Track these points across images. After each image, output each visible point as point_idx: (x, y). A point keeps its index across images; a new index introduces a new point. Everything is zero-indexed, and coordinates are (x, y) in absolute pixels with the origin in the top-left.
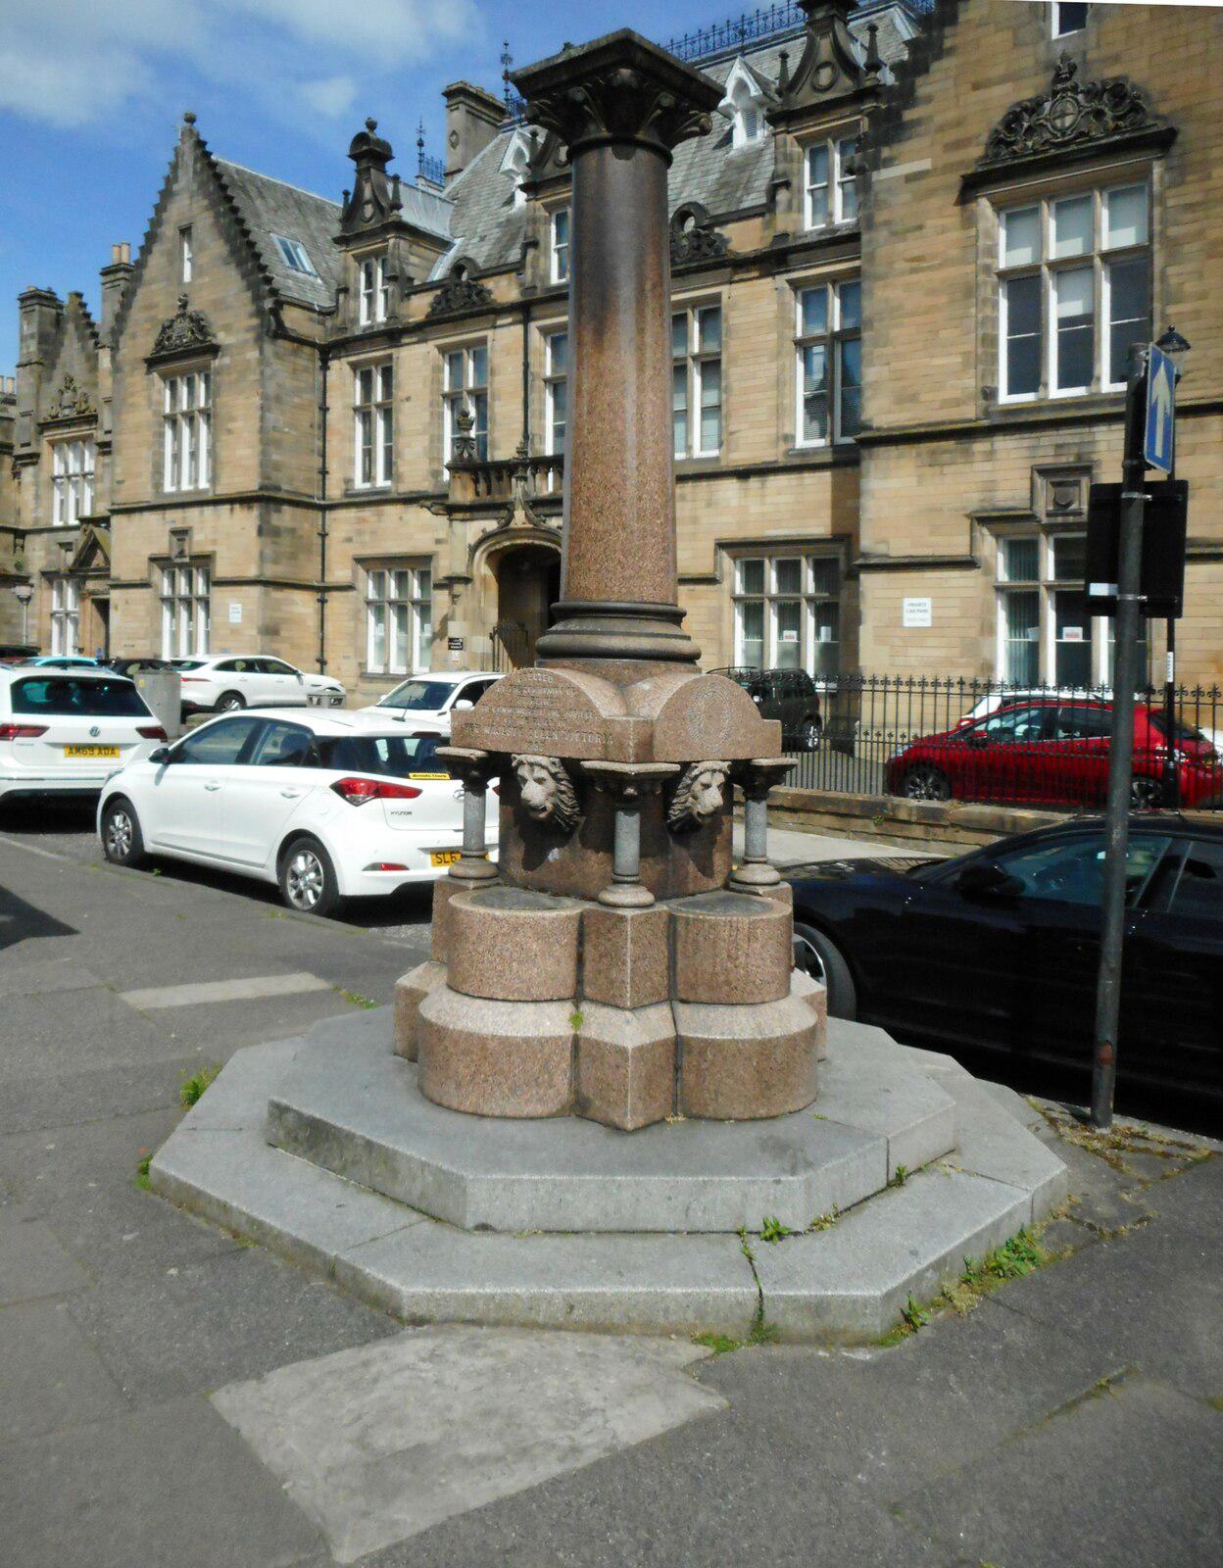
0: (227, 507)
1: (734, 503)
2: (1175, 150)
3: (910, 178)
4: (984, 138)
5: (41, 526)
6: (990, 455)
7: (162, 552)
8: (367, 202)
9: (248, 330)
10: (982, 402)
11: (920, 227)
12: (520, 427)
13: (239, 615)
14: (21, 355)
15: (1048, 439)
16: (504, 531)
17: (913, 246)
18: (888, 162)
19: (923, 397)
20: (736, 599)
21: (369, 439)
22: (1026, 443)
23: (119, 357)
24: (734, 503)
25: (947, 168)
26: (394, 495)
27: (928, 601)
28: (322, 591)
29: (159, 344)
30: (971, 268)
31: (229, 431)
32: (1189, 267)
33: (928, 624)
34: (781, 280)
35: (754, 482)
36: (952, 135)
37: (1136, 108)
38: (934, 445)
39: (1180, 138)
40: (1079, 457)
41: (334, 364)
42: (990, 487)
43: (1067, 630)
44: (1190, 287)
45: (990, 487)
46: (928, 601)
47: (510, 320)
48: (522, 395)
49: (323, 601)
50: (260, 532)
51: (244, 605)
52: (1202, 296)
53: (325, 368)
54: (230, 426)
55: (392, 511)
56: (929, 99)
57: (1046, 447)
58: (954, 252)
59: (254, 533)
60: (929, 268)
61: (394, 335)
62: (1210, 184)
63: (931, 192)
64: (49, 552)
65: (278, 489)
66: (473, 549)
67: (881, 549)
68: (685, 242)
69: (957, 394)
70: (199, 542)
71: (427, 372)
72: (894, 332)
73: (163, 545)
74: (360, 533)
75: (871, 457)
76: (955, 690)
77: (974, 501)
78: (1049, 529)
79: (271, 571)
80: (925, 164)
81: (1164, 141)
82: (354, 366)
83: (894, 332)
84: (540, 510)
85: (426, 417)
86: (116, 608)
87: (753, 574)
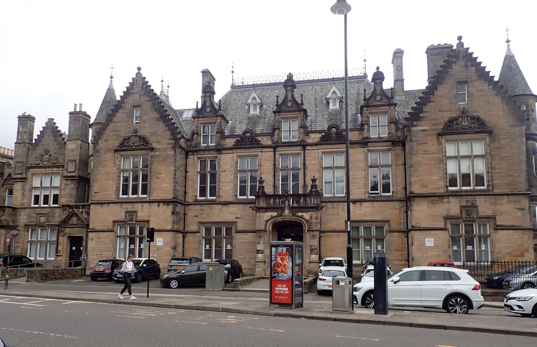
0: (157, 204)
2: (492, 135)
3: (422, 131)
4: (443, 124)
6: (449, 202)
8: (208, 107)
10: (446, 189)
11: (426, 143)
15: (464, 199)
16: (280, 215)
17: (424, 147)
18: (416, 126)
19: (429, 186)
22: (458, 200)
23: (98, 147)
26: (218, 202)
27: (433, 239)
28: (185, 234)
29: (122, 144)
30: (441, 155)
31: (158, 178)
33: (433, 245)
36: (434, 122)
37: (483, 124)
38: (433, 198)
40: (472, 204)
41: (191, 157)
43: (468, 247)
44: (497, 166)
45: (449, 210)
46: (433, 239)
48: (273, 173)
49: (184, 237)
50: (173, 213)
52: (501, 169)
53: (187, 158)
54: (158, 176)
56: (427, 112)
57: (464, 201)
58: (436, 151)
59: (170, 214)
60: (429, 154)
61: (219, 150)
62: (501, 143)
63: (429, 135)
64: (29, 216)
65: (177, 199)
66: (267, 221)
67: (418, 225)
68: (334, 135)
69: (439, 186)
71: (233, 163)
72: (419, 169)
73: (121, 216)
74: (201, 214)
75: (414, 201)
76: (532, 264)
77: (445, 213)
78: (464, 221)
79: (176, 227)
80: (427, 128)
81: (490, 133)
82: (199, 158)
83: (419, 169)
84: (294, 210)
85: (232, 178)
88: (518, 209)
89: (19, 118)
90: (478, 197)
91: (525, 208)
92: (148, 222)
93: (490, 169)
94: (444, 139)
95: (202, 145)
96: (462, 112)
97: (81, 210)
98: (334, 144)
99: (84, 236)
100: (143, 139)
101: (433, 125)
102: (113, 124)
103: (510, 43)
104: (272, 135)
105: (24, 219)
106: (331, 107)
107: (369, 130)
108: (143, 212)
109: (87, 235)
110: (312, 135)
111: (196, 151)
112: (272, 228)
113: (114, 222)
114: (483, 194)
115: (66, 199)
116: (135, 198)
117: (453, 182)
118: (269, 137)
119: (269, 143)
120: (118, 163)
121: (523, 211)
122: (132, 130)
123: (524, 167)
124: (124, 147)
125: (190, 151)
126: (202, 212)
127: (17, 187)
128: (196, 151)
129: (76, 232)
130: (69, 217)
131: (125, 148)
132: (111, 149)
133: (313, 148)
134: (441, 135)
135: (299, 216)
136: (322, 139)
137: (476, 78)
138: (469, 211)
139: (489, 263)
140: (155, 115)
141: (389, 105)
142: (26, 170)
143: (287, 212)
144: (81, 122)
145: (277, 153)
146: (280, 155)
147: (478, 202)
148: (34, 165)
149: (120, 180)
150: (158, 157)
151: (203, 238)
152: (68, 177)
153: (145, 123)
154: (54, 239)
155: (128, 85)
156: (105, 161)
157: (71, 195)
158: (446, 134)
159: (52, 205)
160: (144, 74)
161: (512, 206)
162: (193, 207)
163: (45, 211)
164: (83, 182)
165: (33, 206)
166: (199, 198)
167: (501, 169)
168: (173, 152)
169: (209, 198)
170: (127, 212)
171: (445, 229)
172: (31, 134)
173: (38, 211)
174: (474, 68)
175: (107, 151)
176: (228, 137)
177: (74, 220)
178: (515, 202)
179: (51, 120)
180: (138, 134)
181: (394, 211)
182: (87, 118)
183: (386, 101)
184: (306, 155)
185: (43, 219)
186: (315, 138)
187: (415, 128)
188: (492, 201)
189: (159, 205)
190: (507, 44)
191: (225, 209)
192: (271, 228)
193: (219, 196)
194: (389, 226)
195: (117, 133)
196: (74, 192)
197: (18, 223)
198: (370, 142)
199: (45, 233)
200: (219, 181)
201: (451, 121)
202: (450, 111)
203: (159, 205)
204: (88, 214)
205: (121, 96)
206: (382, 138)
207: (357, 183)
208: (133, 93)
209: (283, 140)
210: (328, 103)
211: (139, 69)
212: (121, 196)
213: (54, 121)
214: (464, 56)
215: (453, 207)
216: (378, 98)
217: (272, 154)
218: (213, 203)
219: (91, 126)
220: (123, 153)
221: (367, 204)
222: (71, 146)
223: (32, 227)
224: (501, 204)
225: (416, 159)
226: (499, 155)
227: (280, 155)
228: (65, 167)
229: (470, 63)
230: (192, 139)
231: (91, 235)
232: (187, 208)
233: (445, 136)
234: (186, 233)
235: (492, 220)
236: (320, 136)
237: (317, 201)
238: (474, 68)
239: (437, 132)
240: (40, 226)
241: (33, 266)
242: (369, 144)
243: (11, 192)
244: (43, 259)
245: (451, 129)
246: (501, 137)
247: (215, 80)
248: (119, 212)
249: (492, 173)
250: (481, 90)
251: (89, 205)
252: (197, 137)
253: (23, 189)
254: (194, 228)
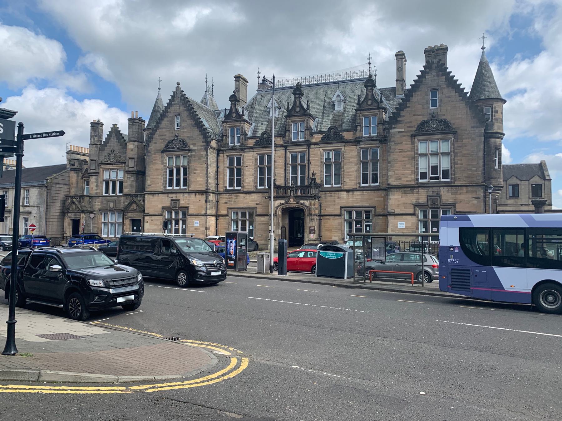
1: (345, 198)
3: (399, 132)
4: (416, 126)
5: (99, 195)
6: (418, 192)
9: (202, 146)
12: (283, 176)
14: (91, 141)
15: (431, 189)
17: (399, 147)
18: (394, 128)
20: (345, 220)
21: (232, 174)
23: (149, 149)
24: (345, 198)
25: (408, 132)
29: (167, 147)
31: (194, 173)
32: (459, 158)
34: (358, 147)
35: (350, 193)
36: (408, 125)
37: (449, 126)
38: (405, 189)
41: (221, 155)
42: (418, 199)
44: (459, 162)
49: (217, 220)
52: (462, 164)
53: (218, 156)
55: (242, 195)
56: (404, 116)
57: (430, 191)
58: (410, 149)
61: (243, 149)
63: (404, 136)
64: (102, 203)
66: (277, 208)
67: (393, 211)
70: (183, 203)
71: (253, 159)
73: (167, 203)
74: (230, 201)
77: (414, 201)
80: (403, 130)
81: (455, 133)
82: (227, 156)
83: (395, 165)
84: (298, 198)
87: (350, 214)
88: (475, 198)
89: (92, 124)
90: (442, 188)
91: (480, 196)
92: (188, 208)
93: (453, 163)
94: (416, 140)
95: (230, 145)
96: (432, 116)
97: (139, 198)
98: (332, 143)
99: (142, 219)
100: (445, 123)
101: (408, 127)
102: (160, 130)
103: (485, 50)
104: (284, 136)
105: (98, 205)
106: (336, 108)
107: (361, 130)
108: (184, 200)
109: (144, 218)
110: (316, 136)
111: (226, 150)
112: (282, 213)
113: (163, 208)
114: (446, 185)
116: (177, 189)
117: (424, 176)
118: (281, 138)
119: (282, 143)
120: (165, 162)
121: (478, 200)
122: (174, 135)
123: (481, 163)
124: (168, 149)
125: (222, 150)
126: (230, 200)
127: (93, 179)
128: (226, 150)
129: (136, 216)
130: (130, 204)
131: (169, 149)
132: (159, 150)
133: (316, 146)
134: (414, 136)
135: (301, 204)
136: (323, 139)
137: (445, 86)
138: (435, 198)
139: (358, 244)
140: (190, 122)
141: (378, 109)
142: (98, 166)
143: (292, 200)
144: (137, 127)
145: (288, 151)
146: (290, 152)
147: (442, 192)
148: (104, 162)
149: (166, 175)
150: (194, 156)
151: (232, 220)
152: (129, 171)
153: (183, 129)
154: (121, 221)
155: (170, 98)
156: (155, 160)
157: (131, 186)
158: (418, 135)
159: (118, 194)
160: (182, 88)
161: (470, 195)
162: (224, 196)
163: (113, 199)
164: (140, 174)
165: (104, 194)
166: (228, 188)
167: (462, 164)
168: (205, 153)
169: (236, 188)
170: (172, 200)
171: (414, 214)
172: (101, 136)
173: (108, 198)
174: (444, 77)
175: (157, 151)
176: (250, 138)
177: (134, 206)
178: (472, 192)
179: (115, 125)
180: (179, 138)
181: (380, 199)
182: (143, 123)
183: (376, 105)
184: (310, 152)
185: (112, 205)
186: (318, 138)
187: (393, 131)
188: (453, 191)
189: (195, 195)
190: (482, 50)
191: (247, 196)
192: (280, 213)
193: (244, 187)
194: (375, 211)
195: (163, 137)
196: (134, 184)
197: (94, 209)
198: (361, 141)
199: (114, 216)
200: (243, 175)
201: (423, 124)
202: (422, 115)
203: (195, 195)
204: (144, 201)
205: (167, 103)
206: (372, 137)
207: (351, 175)
208: (175, 104)
209: (293, 140)
210: (334, 105)
211: (178, 84)
212: (168, 188)
213: (118, 126)
214: (436, 67)
215: (422, 196)
216: (370, 102)
217: (283, 152)
218: (239, 192)
219: (144, 130)
220: (420, 138)
221: (358, 193)
222: (130, 146)
223: (105, 211)
224: (460, 194)
225: (392, 157)
226: (461, 152)
227: (290, 152)
228: (127, 163)
229: (441, 73)
230: (222, 140)
231: (146, 218)
232: (219, 196)
233: (417, 137)
234: (219, 216)
235: (453, 207)
236: (322, 136)
237: (316, 191)
238: (444, 77)
239: (411, 133)
240: (110, 211)
241: (104, 242)
242: (361, 143)
243: (88, 184)
244: (113, 236)
245: (422, 131)
246: (464, 137)
247: (247, 82)
248: (166, 201)
249: (454, 167)
250: (449, 97)
251: (144, 195)
252: (226, 139)
253: (97, 181)
254: (224, 212)
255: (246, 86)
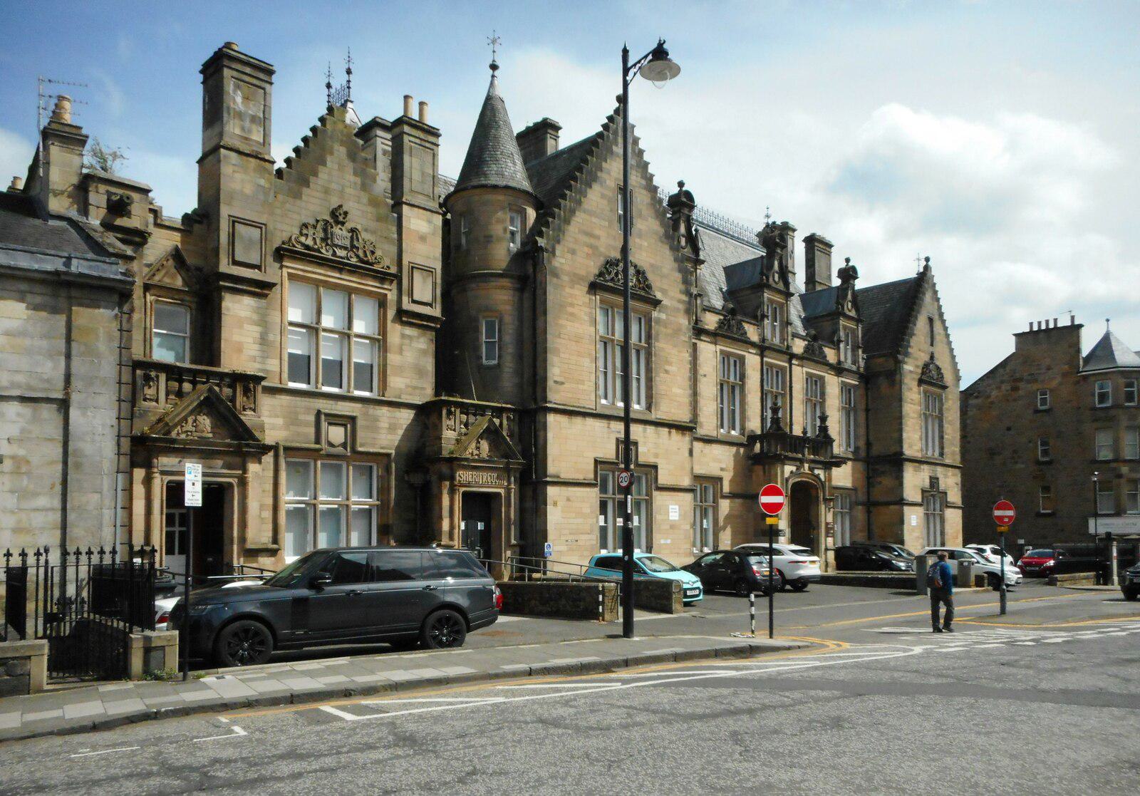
0: (666, 430)
7: (608, 456)
9: (680, 301)
13: (677, 514)
27: (671, 518)
31: (667, 372)
39: (586, 289)
47: (754, 352)
49: (869, 512)
51: (680, 506)
54: (667, 367)
86: (555, 504)
115: (408, 381)
132: (581, 278)
195: (592, 241)
203: (670, 432)
223: (300, 458)
234: (877, 504)
247: (830, 246)
255: (829, 254)
